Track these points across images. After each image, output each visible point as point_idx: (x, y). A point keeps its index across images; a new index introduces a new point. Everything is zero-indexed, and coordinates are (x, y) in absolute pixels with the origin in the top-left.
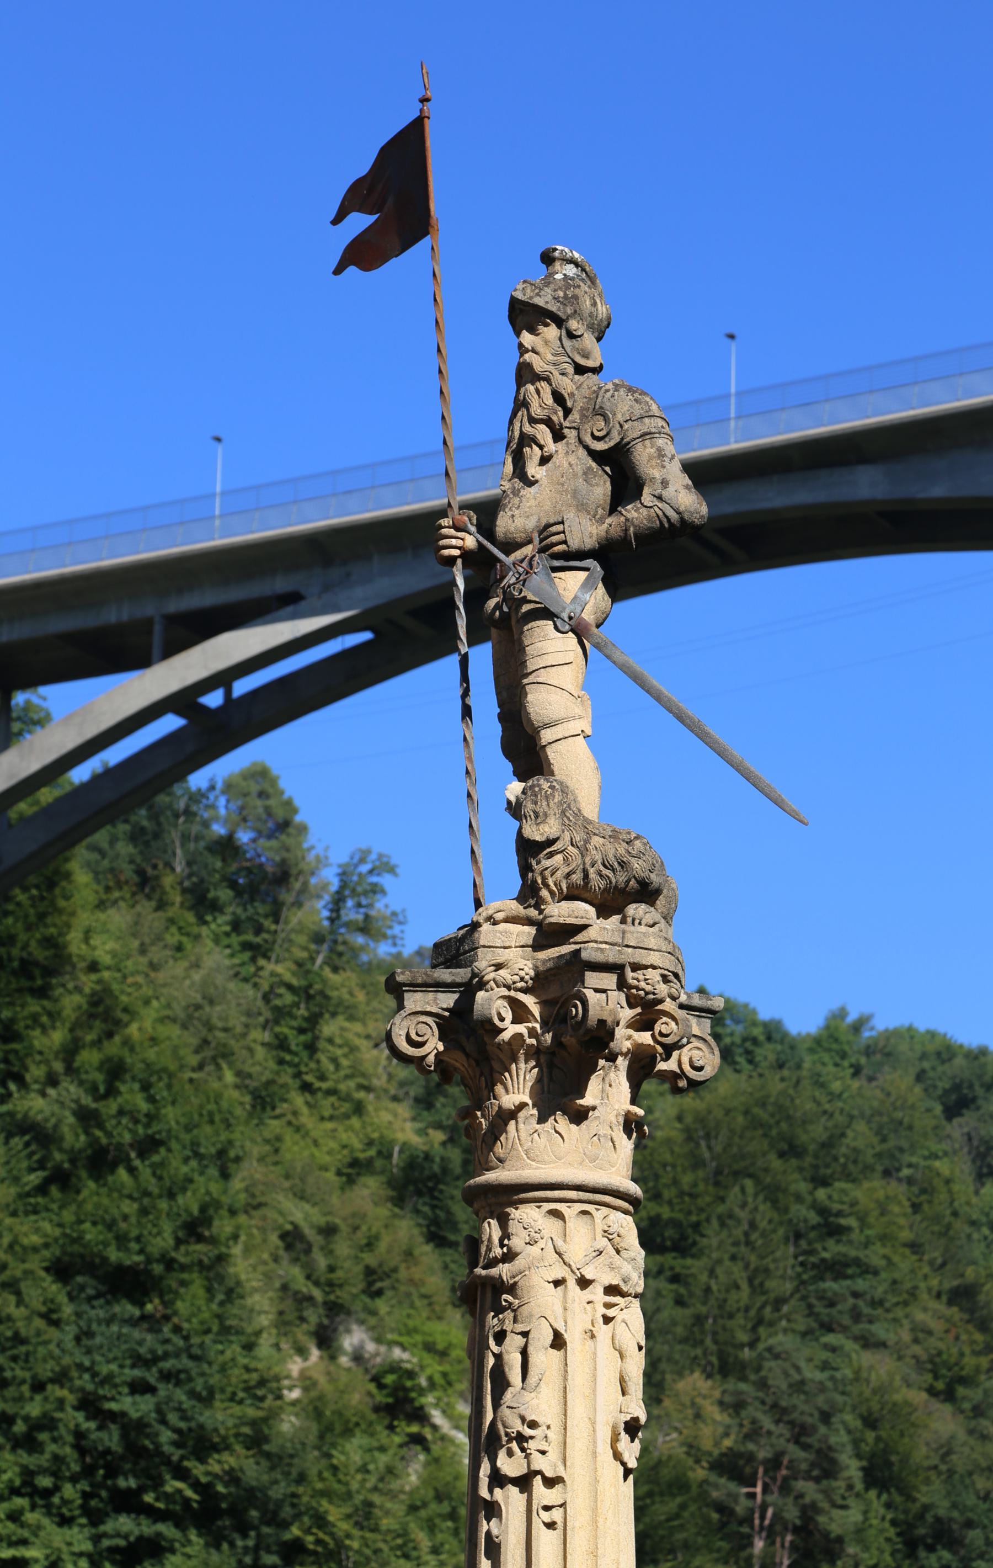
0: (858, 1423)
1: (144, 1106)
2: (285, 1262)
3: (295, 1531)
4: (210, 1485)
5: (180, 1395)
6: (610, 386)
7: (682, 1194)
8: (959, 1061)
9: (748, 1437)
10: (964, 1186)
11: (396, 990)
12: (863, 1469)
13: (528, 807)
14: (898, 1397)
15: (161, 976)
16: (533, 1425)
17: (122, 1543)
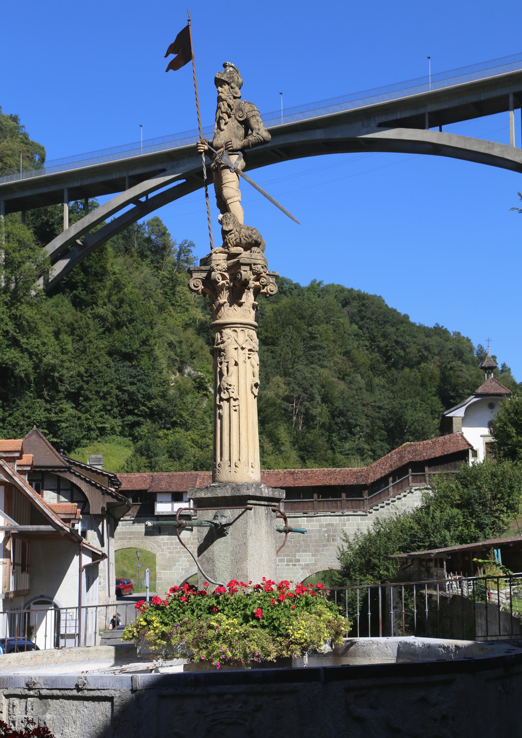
0: (320, 387)
1: (130, 310)
2: (169, 351)
3: (175, 419)
4: (152, 408)
5: (143, 385)
6: (243, 102)
7: (273, 330)
8: (346, 292)
9: (291, 391)
10: (347, 325)
11: (190, 272)
12: (321, 398)
13: (224, 221)
14: (330, 380)
15: (132, 276)
16: (230, 385)
17: (130, 423)
